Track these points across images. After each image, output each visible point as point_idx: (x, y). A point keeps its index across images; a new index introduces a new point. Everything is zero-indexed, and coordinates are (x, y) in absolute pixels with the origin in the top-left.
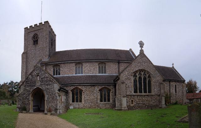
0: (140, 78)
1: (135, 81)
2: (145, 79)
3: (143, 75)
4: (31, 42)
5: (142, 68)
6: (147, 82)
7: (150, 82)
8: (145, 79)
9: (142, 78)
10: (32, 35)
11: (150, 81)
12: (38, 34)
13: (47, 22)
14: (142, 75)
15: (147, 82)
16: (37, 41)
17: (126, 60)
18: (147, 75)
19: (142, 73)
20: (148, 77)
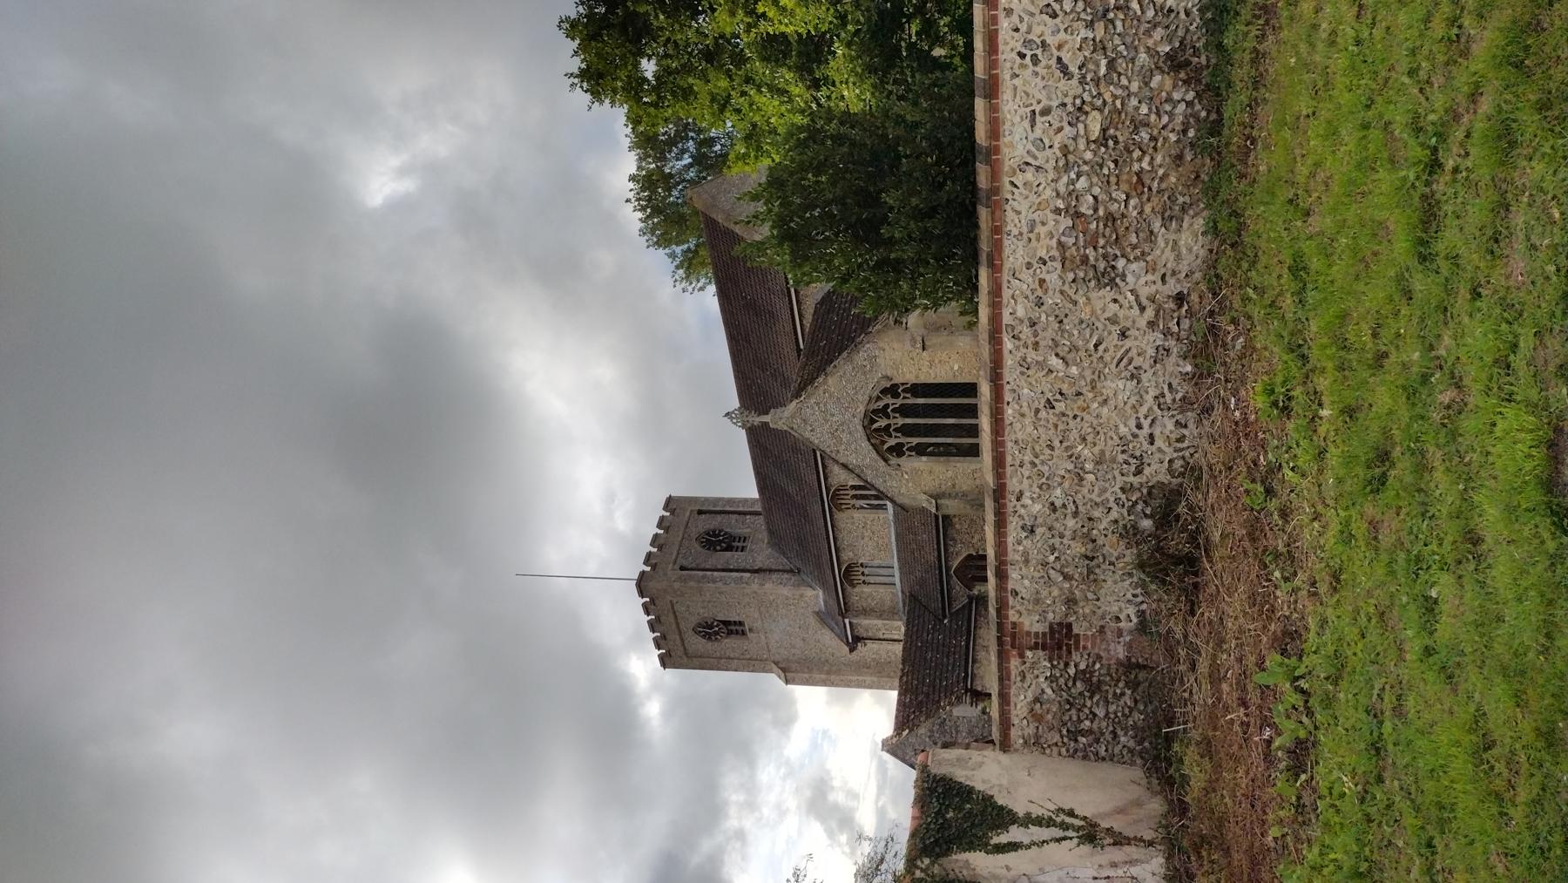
0: (906, 431)
1: (920, 450)
2: (904, 411)
3: (888, 417)
4: (730, 644)
5: (860, 428)
6: (921, 401)
7: (918, 389)
8: (904, 411)
9: (901, 421)
10: (698, 643)
11: (915, 386)
12: (694, 620)
13: (670, 503)
14: (892, 421)
15: (921, 401)
16: (733, 538)
17: (829, 572)
18: (888, 400)
19: (882, 423)
20: (896, 395)
